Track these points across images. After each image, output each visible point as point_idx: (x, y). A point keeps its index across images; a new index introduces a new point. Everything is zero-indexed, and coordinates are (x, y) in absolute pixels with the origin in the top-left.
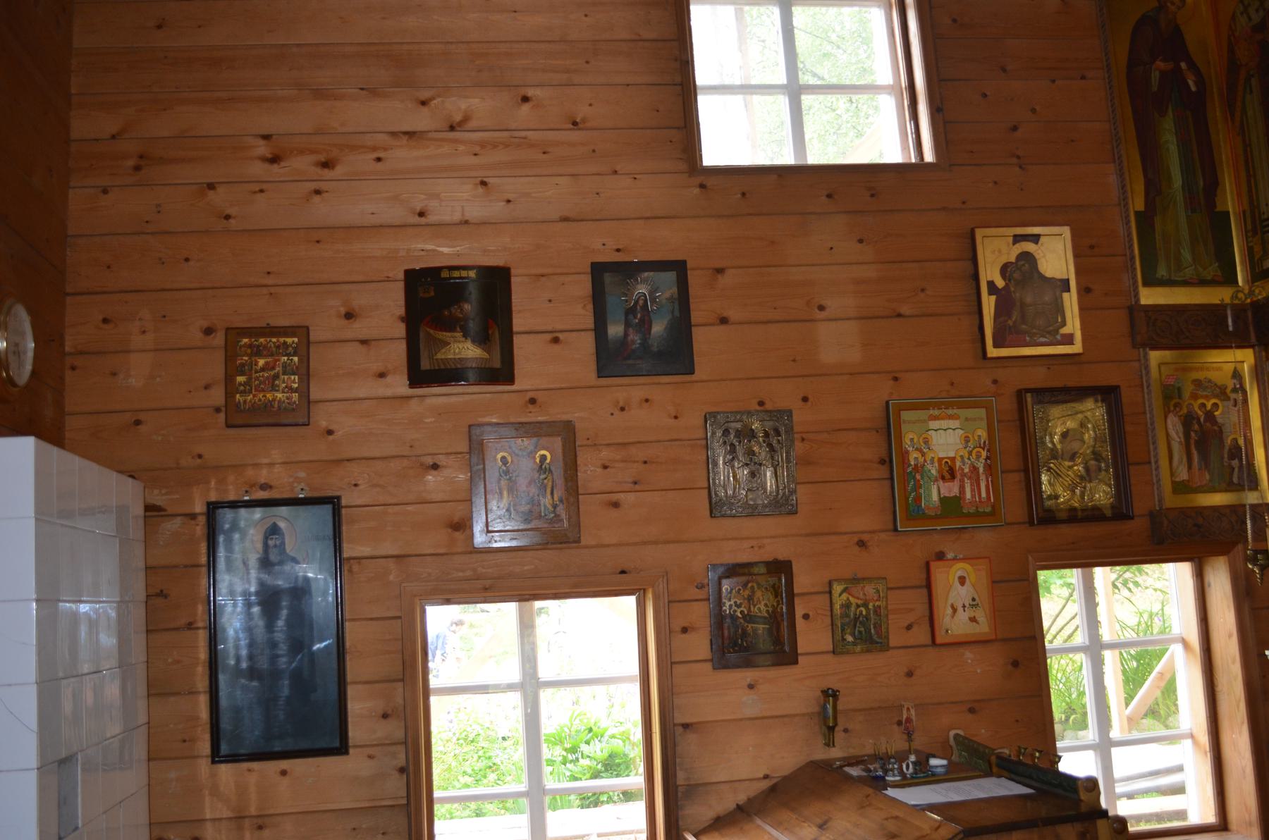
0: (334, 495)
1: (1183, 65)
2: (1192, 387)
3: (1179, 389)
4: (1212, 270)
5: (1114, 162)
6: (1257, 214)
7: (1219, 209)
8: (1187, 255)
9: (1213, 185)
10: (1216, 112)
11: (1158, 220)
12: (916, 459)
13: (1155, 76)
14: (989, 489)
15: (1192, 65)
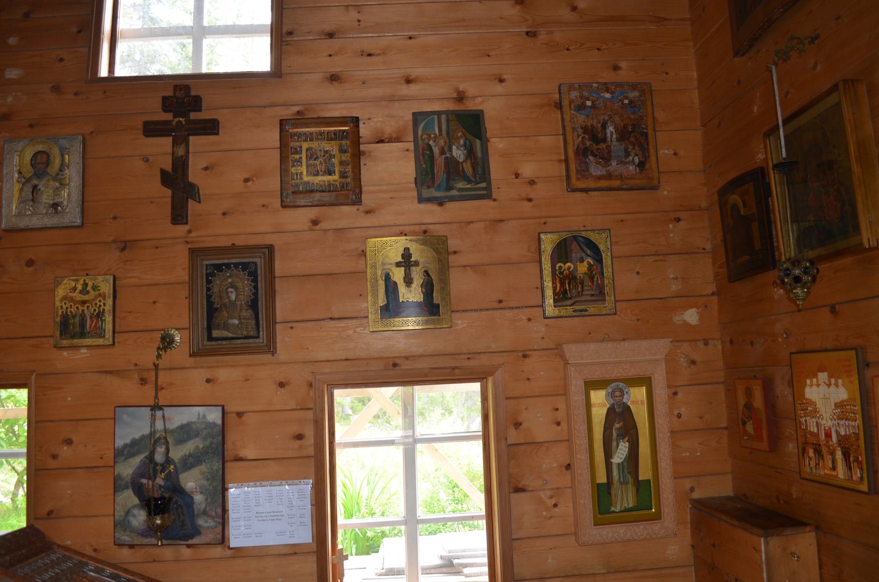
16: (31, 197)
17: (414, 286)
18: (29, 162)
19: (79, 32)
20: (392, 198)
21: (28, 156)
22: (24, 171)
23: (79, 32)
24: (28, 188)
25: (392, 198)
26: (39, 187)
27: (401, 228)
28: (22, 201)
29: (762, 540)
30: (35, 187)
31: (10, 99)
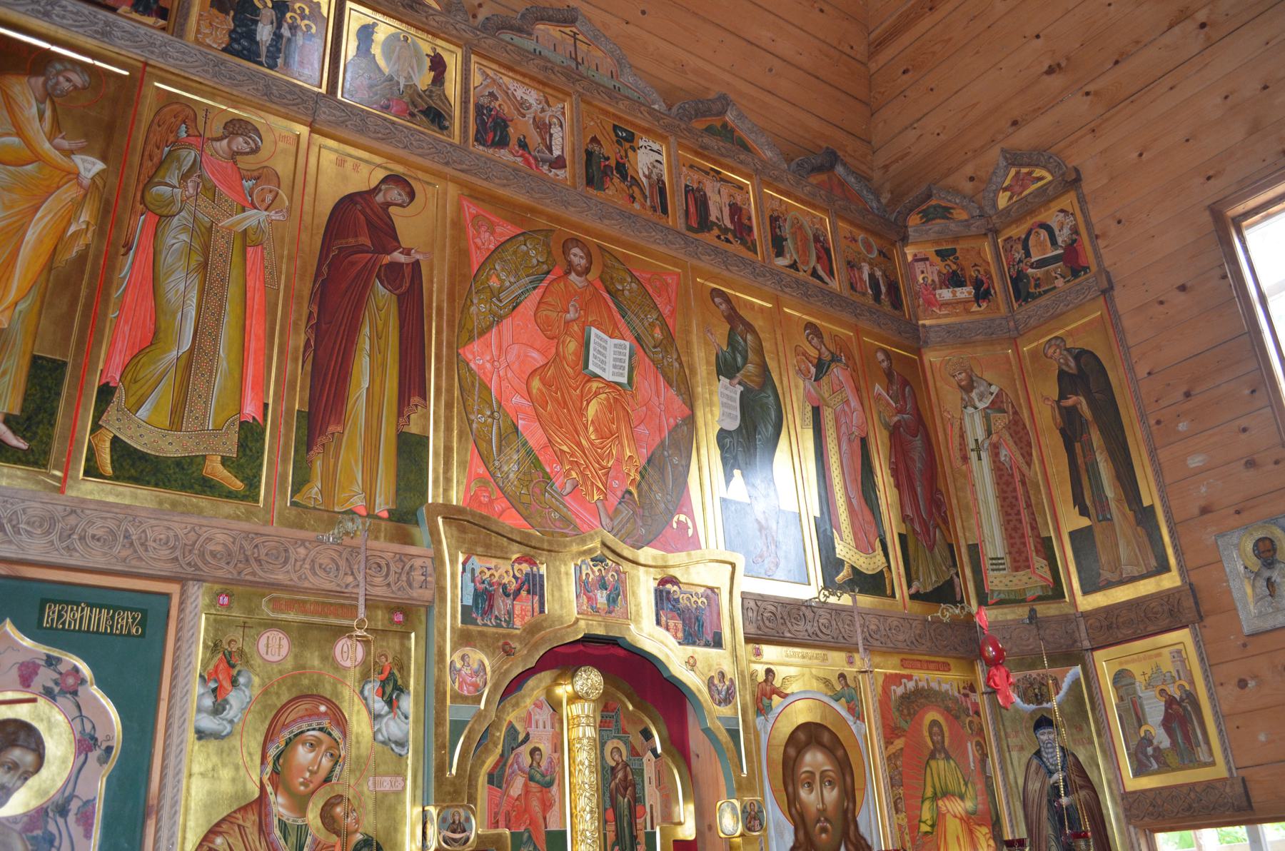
16: (1268, 592)
17: (106, 767)
18: (1252, 554)
19: (1253, 392)
20: (1171, 88)
21: (1249, 546)
22: (1249, 564)
23: (1253, 392)
24: (1261, 583)
25: (1171, 88)
26: (1273, 579)
27: (1088, 127)
28: (1259, 599)
29: (386, 71)
30: (1269, 580)
31: (1203, 490)
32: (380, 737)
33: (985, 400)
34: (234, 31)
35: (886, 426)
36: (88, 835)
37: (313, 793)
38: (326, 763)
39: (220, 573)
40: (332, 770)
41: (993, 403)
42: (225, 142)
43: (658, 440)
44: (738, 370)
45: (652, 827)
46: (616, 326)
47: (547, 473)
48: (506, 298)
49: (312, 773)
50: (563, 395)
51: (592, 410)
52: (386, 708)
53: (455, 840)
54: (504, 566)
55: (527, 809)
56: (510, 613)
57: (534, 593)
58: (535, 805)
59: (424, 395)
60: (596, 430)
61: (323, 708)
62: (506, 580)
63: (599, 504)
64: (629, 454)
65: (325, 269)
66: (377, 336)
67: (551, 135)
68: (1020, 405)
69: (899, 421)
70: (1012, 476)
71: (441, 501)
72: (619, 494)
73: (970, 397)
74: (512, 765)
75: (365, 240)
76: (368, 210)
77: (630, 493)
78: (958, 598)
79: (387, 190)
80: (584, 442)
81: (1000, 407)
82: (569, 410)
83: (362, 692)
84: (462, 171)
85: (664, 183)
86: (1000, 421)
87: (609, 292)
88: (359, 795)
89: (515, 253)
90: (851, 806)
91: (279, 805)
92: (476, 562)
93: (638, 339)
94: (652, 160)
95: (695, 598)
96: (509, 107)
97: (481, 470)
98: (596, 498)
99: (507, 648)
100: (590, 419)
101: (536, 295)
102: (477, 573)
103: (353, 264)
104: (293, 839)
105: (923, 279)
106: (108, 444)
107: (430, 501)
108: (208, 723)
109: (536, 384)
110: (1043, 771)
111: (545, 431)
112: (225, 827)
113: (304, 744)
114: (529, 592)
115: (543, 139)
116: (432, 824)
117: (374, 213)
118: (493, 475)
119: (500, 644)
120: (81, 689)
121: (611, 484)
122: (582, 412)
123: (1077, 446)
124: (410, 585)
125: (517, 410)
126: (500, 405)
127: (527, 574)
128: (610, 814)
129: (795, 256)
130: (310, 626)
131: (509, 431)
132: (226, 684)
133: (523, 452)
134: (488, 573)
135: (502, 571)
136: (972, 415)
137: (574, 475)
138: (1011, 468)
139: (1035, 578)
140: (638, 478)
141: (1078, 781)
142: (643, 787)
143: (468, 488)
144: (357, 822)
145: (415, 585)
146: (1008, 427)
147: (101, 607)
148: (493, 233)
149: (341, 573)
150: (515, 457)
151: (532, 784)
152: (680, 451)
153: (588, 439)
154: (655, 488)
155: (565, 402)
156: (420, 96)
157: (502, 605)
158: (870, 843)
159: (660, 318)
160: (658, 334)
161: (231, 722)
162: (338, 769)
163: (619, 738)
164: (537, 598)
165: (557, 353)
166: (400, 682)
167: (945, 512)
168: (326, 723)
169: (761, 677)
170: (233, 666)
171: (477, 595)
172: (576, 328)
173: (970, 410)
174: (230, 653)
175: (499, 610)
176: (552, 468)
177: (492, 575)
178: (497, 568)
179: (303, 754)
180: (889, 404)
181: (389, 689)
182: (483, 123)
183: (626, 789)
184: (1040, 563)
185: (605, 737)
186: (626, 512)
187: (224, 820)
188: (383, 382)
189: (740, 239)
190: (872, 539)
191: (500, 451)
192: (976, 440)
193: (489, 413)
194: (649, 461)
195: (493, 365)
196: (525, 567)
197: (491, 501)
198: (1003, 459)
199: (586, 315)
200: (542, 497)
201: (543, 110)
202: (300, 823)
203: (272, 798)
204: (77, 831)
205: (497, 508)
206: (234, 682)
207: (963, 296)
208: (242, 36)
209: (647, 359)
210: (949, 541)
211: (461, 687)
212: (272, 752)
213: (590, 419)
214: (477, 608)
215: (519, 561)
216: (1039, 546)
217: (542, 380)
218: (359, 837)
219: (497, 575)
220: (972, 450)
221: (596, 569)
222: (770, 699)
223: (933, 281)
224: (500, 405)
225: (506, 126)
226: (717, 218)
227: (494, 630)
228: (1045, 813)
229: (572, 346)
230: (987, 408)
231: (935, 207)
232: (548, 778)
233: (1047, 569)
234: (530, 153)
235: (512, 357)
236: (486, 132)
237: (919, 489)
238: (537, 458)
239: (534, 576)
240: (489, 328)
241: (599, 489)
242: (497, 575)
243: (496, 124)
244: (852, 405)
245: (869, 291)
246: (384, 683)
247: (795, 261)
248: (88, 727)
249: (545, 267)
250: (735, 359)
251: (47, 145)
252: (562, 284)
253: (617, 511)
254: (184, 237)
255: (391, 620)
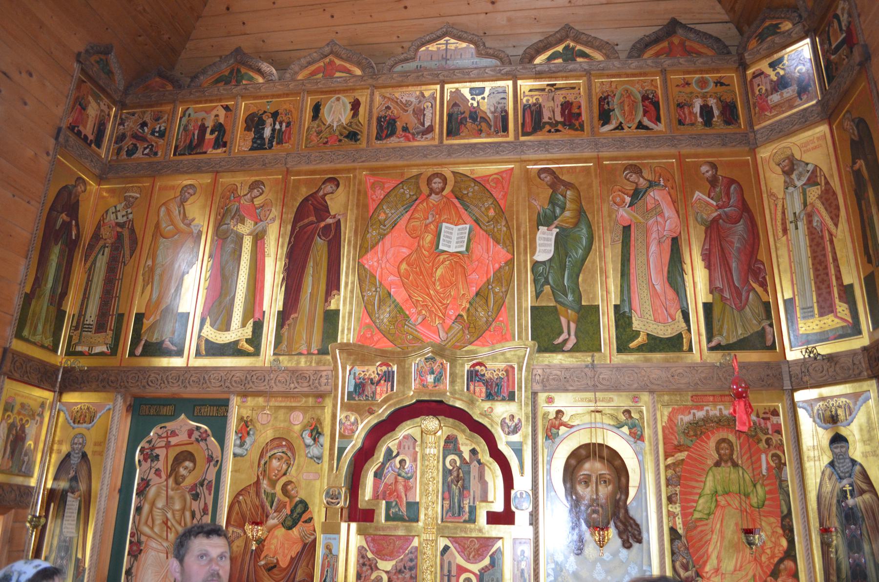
0: (330, 424)
1: (74, 222)
2: (20, 407)
3: (13, 406)
4: (48, 342)
5: (26, 258)
6: (82, 320)
7: (62, 308)
8: (40, 327)
9: (64, 294)
10: (79, 255)
11: (33, 303)
12: (30, 445)
13: (60, 222)
14: (664, 563)
15: (77, 225)
32: (309, 455)
33: (802, 178)
34: (254, 138)
35: (703, 222)
36: (210, 494)
37: (279, 479)
38: (285, 467)
39: (238, 389)
40: (287, 470)
41: (809, 179)
42: (249, 195)
43: (485, 280)
44: (556, 218)
45: (474, 503)
46: (460, 217)
47: (406, 314)
48: (388, 224)
49: (278, 471)
50: (420, 269)
51: (439, 273)
52: (313, 442)
53: (332, 503)
54: (372, 369)
55: (396, 490)
56: (374, 393)
57: (389, 381)
58: (401, 488)
59: (338, 289)
60: (441, 284)
61: (284, 443)
62: (372, 376)
63: (439, 326)
64: (462, 292)
65: (293, 239)
66: (316, 264)
67: (424, 115)
68: (832, 176)
69: (719, 215)
70: (822, 237)
71: (345, 341)
72: (454, 318)
73: (791, 178)
74: (388, 468)
75: (314, 219)
76: (315, 203)
77: (462, 316)
78: (769, 343)
79: (325, 188)
80: (432, 292)
81: (814, 182)
82: (423, 276)
83: (302, 435)
84: (363, 162)
85: (507, 112)
86: (814, 193)
87: (457, 198)
88: (298, 481)
89: (396, 196)
90: (623, 497)
91: (265, 484)
92: (358, 370)
93: (477, 221)
94: (498, 99)
95: (497, 372)
96: (397, 110)
97: (368, 320)
98: (437, 323)
99: (370, 410)
100: (437, 278)
101: (407, 216)
102: (357, 374)
103: (305, 233)
104: (270, 498)
105: (759, 91)
106: (203, 342)
107: (339, 341)
108: (239, 451)
109: (404, 266)
110: (835, 477)
111: (407, 291)
112: (243, 492)
113: (275, 458)
114: (385, 381)
115: (419, 120)
116: (812, 509)
117: (318, 202)
118: (374, 322)
119: (367, 408)
120: (208, 439)
121: (448, 313)
122: (431, 275)
123: (863, 202)
124: (320, 385)
125: (391, 283)
126: (381, 283)
127: (385, 372)
128: (447, 494)
129: (621, 119)
130: (280, 407)
131: (386, 296)
132: (245, 435)
133: (393, 306)
134: (363, 374)
135: (371, 372)
136: (792, 194)
137: (424, 312)
138: (822, 231)
139: (836, 320)
140: (468, 306)
141: (864, 486)
142: (470, 481)
143: (360, 331)
144: (297, 493)
145: (323, 384)
146: (820, 197)
147: (214, 406)
148: (383, 189)
149: (288, 383)
150: (388, 310)
151: (399, 478)
152: (502, 283)
153: (435, 290)
154: (479, 309)
155: (421, 272)
156: (345, 128)
157: (369, 389)
158: (639, 522)
159: (495, 202)
160: (492, 213)
161: (247, 450)
162: (290, 469)
163: (456, 454)
164: (390, 384)
165: (419, 245)
166: (319, 430)
167: (764, 278)
168: (285, 449)
169: (552, 416)
170: (248, 427)
171: (356, 385)
172: (432, 227)
173: (791, 189)
174: (247, 422)
175: (368, 392)
176: (410, 312)
177: (365, 374)
178: (368, 371)
179: (275, 463)
180: (708, 204)
181: (314, 433)
182: (381, 126)
183: (458, 482)
184: (842, 309)
185: (446, 453)
186: (457, 327)
187: (243, 490)
188: (318, 288)
189: (569, 125)
190: (672, 311)
191: (379, 308)
192: (795, 214)
193: (374, 289)
194: (477, 294)
195: (378, 263)
196: (384, 368)
197: (372, 336)
198: (815, 224)
199: (440, 217)
200: (402, 329)
201: (420, 102)
202: (273, 492)
203: (261, 481)
204: (207, 492)
205: (375, 339)
206: (248, 434)
207: (788, 95)
208: (258, 139)
209: (481, 232)
210: (765, 299)
211: (344, 431)
212: (263, 462)
213: (437, 278)
214: (356, 392)
215: (381, 365)
216: (842, 293)
217: (408, 264)
218: (297, 499)
219: (368, 374)
220: (791, 222)
221: (428, 364)
222: (558, 429)
223: (766, 90)
224: (381, 283)
225: (395, 122)
226: (550, 118)
227: (364, 402)
228: (834, 509)
229: (429, 238)
230: (804, 184)
231: (767, 28)
232: (409, 475)
233: (847, 312)
234: (409, 132)
235: (390, 255)
236: (382, 132)
237: (734, 265)
238: (401, 308)
239: (389, 372)
240: (377, 243)
241: (439, 317)
242: (368, 374)
243: (389, 123)
244: (666, 215)
245: (700, 120)
246: (312, 431)
247: (621, 123)
248: (210, 453)
249: (415, 197)
250: (554, 212)
251: (182, 225)
252: (425, 204)
253: (451, 328)
254: (232, 246)
255: (316, 402)
